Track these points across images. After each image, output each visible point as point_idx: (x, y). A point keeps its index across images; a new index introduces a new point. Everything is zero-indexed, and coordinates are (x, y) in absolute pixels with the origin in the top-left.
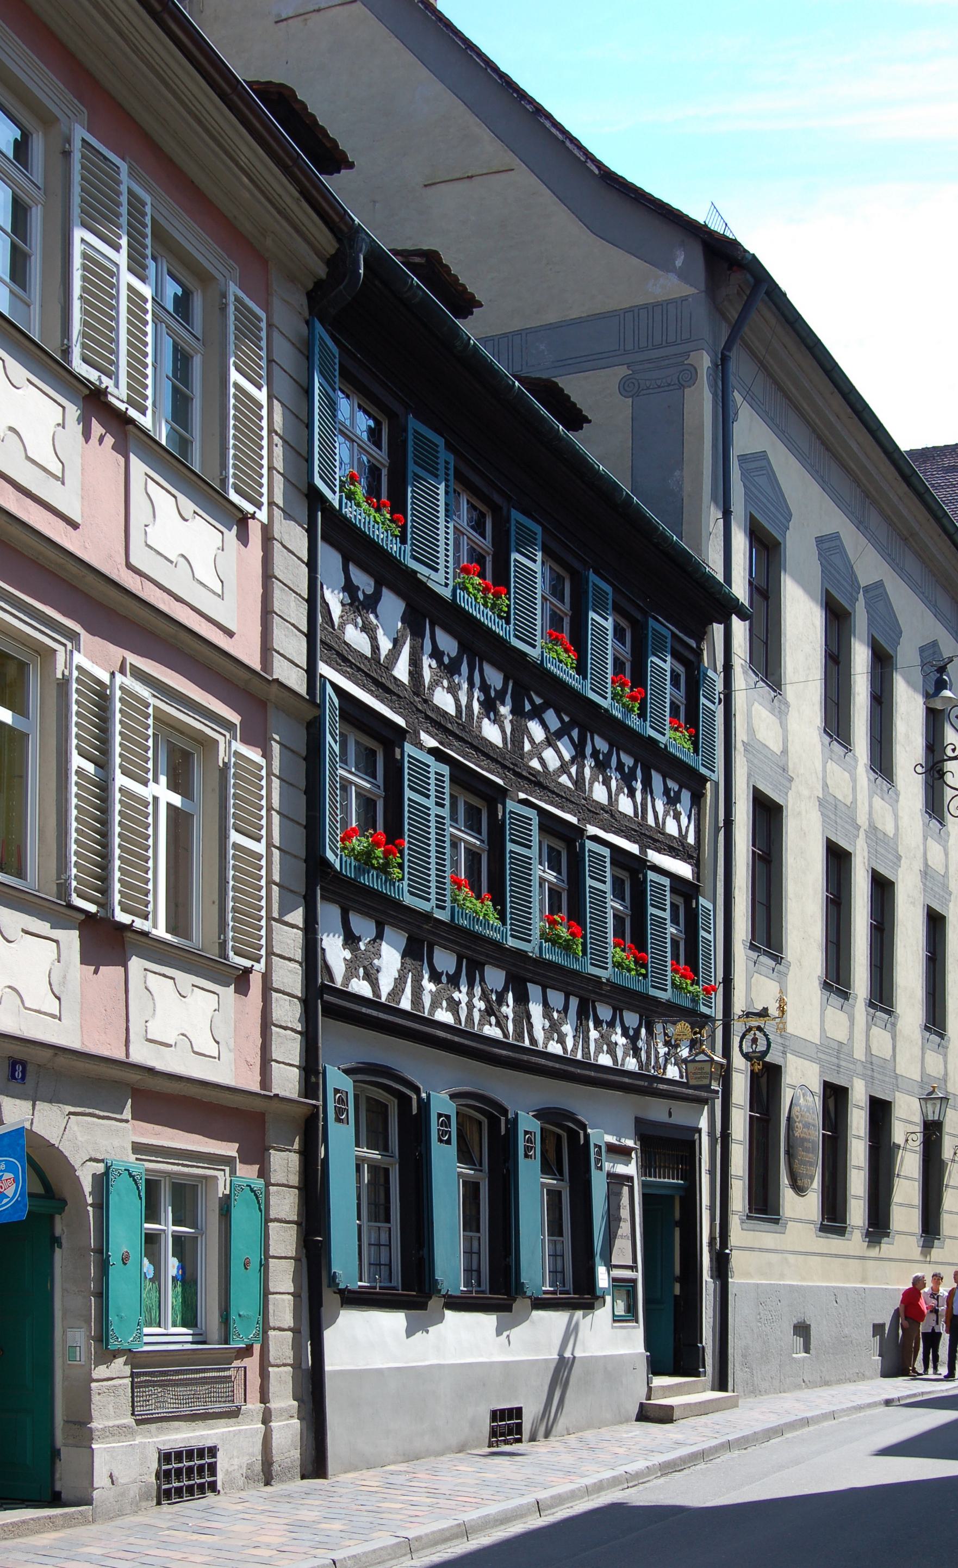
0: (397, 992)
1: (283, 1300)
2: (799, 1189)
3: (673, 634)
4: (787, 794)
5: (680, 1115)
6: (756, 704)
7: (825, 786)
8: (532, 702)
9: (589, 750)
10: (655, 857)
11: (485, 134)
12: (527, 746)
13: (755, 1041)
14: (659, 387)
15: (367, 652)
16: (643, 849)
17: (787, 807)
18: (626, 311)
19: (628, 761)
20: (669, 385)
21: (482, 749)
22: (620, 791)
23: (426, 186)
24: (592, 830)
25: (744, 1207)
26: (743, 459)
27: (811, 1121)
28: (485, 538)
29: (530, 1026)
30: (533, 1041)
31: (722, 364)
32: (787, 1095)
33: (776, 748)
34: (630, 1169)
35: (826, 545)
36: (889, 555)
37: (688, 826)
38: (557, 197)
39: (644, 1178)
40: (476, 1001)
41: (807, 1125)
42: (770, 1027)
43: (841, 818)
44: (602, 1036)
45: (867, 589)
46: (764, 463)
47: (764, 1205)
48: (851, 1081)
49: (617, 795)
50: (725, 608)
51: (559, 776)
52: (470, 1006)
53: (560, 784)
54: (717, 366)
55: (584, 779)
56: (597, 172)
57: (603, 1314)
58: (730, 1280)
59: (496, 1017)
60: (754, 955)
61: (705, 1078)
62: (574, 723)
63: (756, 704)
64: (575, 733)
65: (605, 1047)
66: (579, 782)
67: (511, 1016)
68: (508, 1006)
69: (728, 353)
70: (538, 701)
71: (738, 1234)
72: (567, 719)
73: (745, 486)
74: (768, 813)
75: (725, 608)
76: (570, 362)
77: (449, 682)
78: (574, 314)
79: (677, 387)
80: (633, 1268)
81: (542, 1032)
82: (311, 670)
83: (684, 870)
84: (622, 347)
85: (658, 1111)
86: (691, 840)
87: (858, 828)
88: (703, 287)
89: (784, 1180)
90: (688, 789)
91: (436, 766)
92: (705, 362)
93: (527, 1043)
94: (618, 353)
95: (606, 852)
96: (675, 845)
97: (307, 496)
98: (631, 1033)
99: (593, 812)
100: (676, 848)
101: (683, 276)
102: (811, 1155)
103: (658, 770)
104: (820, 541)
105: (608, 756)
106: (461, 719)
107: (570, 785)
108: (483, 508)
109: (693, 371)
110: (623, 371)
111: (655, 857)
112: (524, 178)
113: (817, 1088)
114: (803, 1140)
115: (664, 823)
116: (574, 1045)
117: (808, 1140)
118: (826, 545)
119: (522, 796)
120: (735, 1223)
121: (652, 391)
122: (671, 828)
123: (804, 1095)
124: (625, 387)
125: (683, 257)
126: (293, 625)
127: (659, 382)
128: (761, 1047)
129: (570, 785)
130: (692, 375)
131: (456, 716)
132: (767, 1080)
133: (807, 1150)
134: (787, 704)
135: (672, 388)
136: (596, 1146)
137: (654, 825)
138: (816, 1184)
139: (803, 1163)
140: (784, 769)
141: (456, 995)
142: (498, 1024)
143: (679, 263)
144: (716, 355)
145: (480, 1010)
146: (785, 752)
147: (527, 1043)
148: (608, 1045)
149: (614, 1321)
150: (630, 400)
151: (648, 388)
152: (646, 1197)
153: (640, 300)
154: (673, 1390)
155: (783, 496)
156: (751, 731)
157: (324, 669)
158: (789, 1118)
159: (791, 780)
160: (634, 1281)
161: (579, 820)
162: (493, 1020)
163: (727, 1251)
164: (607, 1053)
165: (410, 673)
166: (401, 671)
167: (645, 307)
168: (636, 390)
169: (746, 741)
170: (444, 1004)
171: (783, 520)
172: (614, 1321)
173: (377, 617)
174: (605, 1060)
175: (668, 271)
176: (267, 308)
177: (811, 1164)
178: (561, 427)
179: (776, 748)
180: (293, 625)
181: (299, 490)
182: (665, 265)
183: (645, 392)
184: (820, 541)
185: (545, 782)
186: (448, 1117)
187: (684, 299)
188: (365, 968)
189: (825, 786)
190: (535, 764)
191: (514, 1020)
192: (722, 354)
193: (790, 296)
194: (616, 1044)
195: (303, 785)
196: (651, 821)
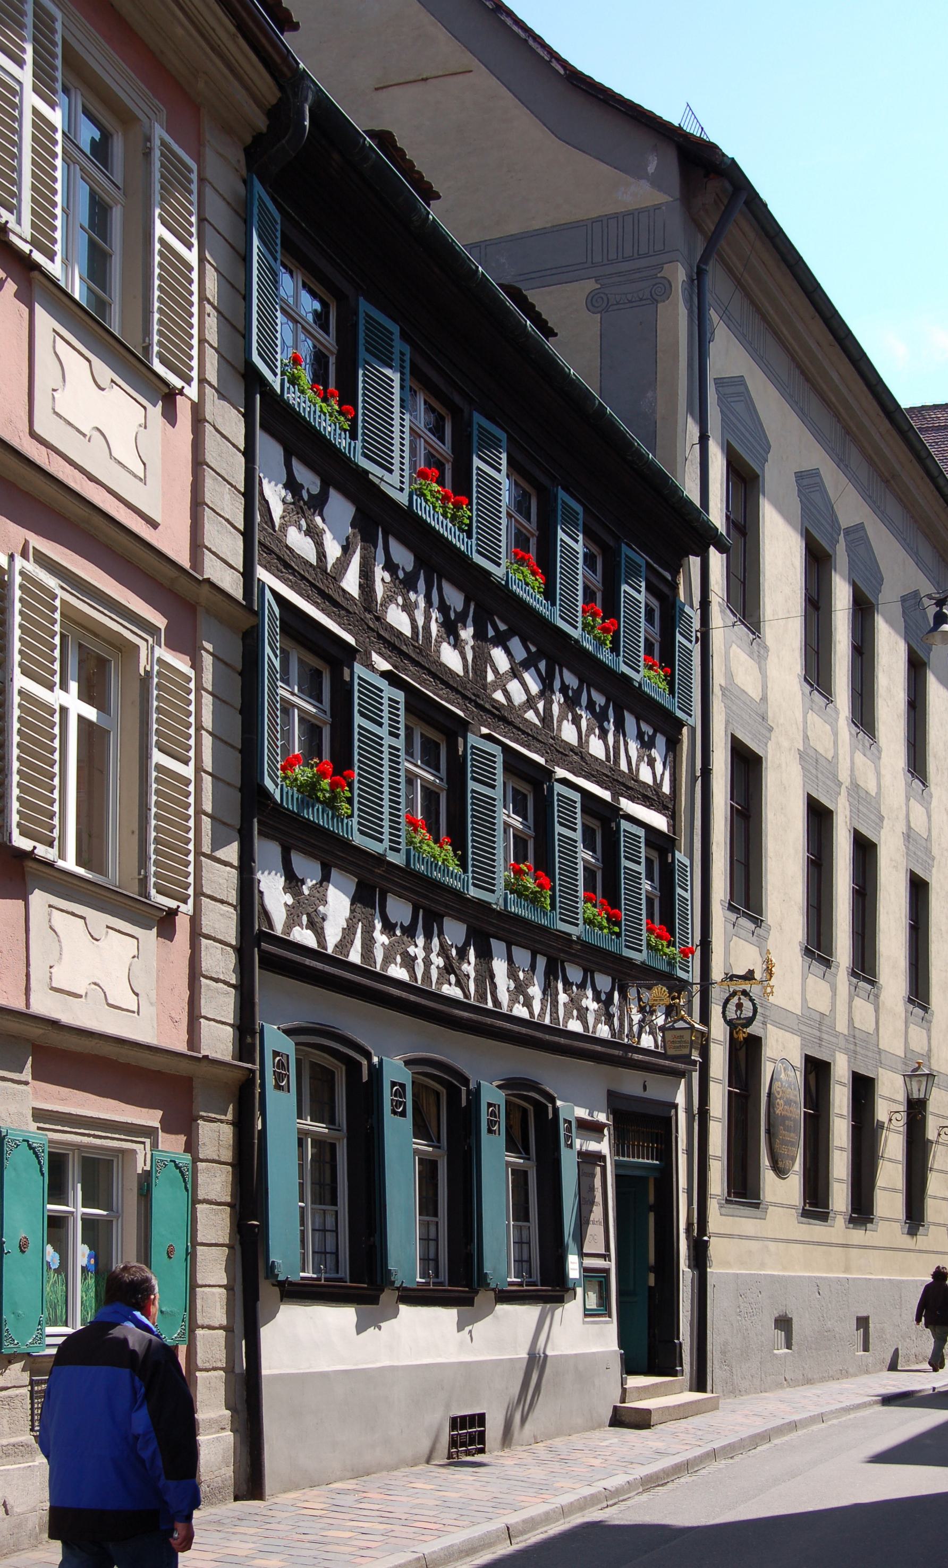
0: (345, 943)
1: (213, 1294)
2: (780, 1171)
3: (647, 562)
4: (766, 745)
5: (656, 1089)
6: (734, 646)
7: (806, 737)
8: (495, 628)
9: (557, 684)
10: (627, 805)
11: (442, 34)
12: (490, 677)
13: (739, 1006)
14: (630, 302)
15: (313, 559)
16: (615, 796)
17: (766, 758)
18: (594, 221)
19: (599, 699)
20: (641, 300)
21: (441, 675)
22: (590, 731)
23: (377, 89)
24: (561, 773)
25: (723, 1190)
26: (719, 382)
27: (792, 1097)
28: (444, 444)
29: (494, 987)
30: (496, 1002)
31: (698, 278)
32: (767, 1070)
33: (755, 694)
34: (603, 1147)
35: (805, 482)
36: (870, 497)
37: (663, 774)
38: (520, 100)
39: (617, 1158)
40: (433, 957)
41: (789, 1102)
42: (755, 990)
43: (822, 773)
44: (572, 1000)
45: (848, 532)
46: (742, 389)
47: (744, 1189)
48: (834, 1056)
49: (588, 736)
50: (701, 538)
51: (525, 712)
52: (428, 963)
53: (526, 720)
54: (693, 281)
55: (552, 716)
56: (562, 72)
57: (572, 1309)
58: (708, 1270)
59: (456, 976)
60: (733, 916)
61: (685, 1047)
62: (541, 654)
63: (734, 646)
64: (542, 665)
65: (575, 1013)
66: (546, 718)
67: (473, 975)
68: (469, 963)
69: (704, 267)
70: (502, 627)
71: (717, 1219)
72: (533, 649)
73: (721, 411)
74: (747, 765)
75: (701, 538)
76: (533, 275)
77: (404, 599)
78: (537, 225)
79: (648, 302)
80: (606, 1257)
81: (507, 994)
82: (248, 574)
83: (659, 821)
84: (589, 260)
85: (631, 1084)
86: (666, 789)
87: (840, 784)
88: (677, 194)
89: (765, 1161)
90: (663, 733)
91: (389, 692)
92: (680, 275)
93: (490, 1005)
94: (586, 266)
95: (577, 797)
96: (649, 794)
97: (244, 376)
98: (603, 997)
99: (562, 752)
100: (650, 797)
101: (657, 182)
102: (792, 1135)
103: (632, 712)
104: (800, 476)
105: (578, 692)
106: (417, 641)
107: (537, 722)
108: (443, 411)
109: (667, 286)
110: (591, 285)
111: (627, 805)
112: (484, 80)
113: (798, 1062)
114: (785, 1118)
115: (638, 770)
116: (542, 1009)
117: (789, 1118)
118: (805, 482)
119: (484, 731)
120: (713, 1207)
121: (622, 306)
122: (645, 775)
123: (785, 1069)
124: (594, 303)
125: (655, 162)
126: (227, 520)
127: (629, 297)
128: (747, 1012)
129: (537, 722)
130: (667, 286)
131: (412, 638)
132: (746, 1052)
133: (788, 1129)
134: (766, 648)
135: (644, 302)
136: (566, 1121)
137: (627, 771)
138: (798, 1166)
139: (784, 1143)
140: (764, 718)
141: (412, 950)
142: (458, 983)
143: (651, 169)
144: (691, 267)
145: (438, 967)
146: (764, 699)
147: (490, 1005)
148: (578, 1010)
149: (586, 1315)
150: (599, 316)
151: (618, 303)
152: (619, 1178)
153: (609, 209)
154: (654, 1393)
155: (764, 431)
156: (729, 675)
157: (262, 574)
158: (770, 1094)
159: (771, 729)
160: (607, 1271)
161: (546, 761)
162: (453, 978)
163: (706, 1238)
164: (578, 1018)
165: (361, 586)
166: (351, 583)
167: (615, 216)
168: (604, 305)
169: (723, 685)
170: (399, 959)
171: (761, 451)
172: (586, 1315)
173: (323, 520)
174: (575, 1026)
175: (640, 178)
176: (199, 158)
177: (793, 1144)
178: (528, 322)
179: (755, 694)
180: (227, 520)
181: (239, 373)
182: (637, 172)
183: (615, 307)
184: (800, 476)
185: (511, 717)
186: (403, 1086)
187: (657, 208)
188: (308, 915)
189: (806, 737)
190: (499, 696)
191: (476, 980)
192: (698, 267)
193: (771, 208)
194: (587, 1009)
195: (238, 703)
196: (624, 767)
